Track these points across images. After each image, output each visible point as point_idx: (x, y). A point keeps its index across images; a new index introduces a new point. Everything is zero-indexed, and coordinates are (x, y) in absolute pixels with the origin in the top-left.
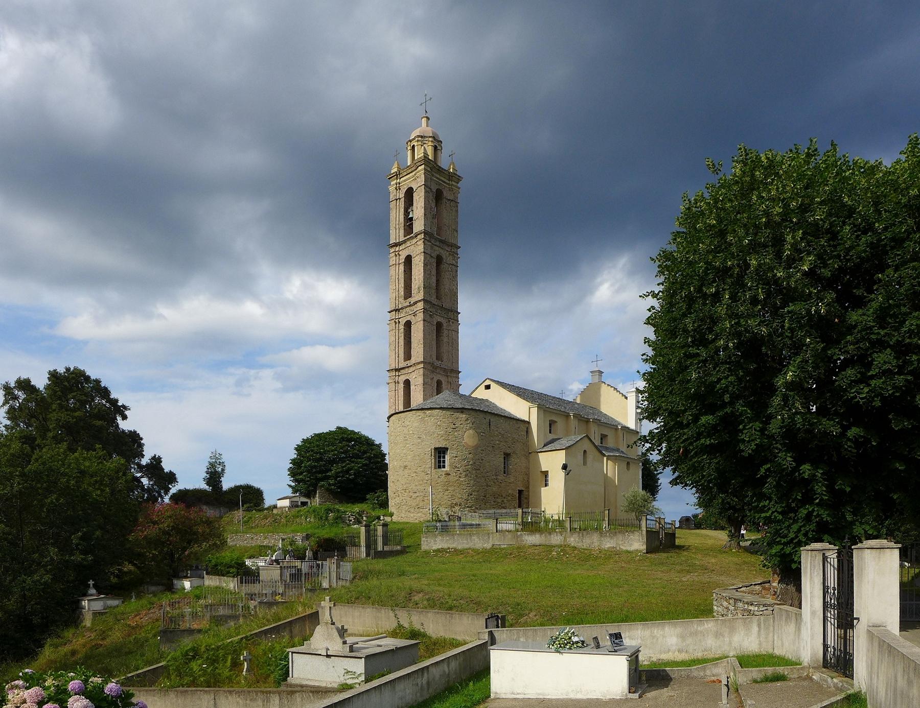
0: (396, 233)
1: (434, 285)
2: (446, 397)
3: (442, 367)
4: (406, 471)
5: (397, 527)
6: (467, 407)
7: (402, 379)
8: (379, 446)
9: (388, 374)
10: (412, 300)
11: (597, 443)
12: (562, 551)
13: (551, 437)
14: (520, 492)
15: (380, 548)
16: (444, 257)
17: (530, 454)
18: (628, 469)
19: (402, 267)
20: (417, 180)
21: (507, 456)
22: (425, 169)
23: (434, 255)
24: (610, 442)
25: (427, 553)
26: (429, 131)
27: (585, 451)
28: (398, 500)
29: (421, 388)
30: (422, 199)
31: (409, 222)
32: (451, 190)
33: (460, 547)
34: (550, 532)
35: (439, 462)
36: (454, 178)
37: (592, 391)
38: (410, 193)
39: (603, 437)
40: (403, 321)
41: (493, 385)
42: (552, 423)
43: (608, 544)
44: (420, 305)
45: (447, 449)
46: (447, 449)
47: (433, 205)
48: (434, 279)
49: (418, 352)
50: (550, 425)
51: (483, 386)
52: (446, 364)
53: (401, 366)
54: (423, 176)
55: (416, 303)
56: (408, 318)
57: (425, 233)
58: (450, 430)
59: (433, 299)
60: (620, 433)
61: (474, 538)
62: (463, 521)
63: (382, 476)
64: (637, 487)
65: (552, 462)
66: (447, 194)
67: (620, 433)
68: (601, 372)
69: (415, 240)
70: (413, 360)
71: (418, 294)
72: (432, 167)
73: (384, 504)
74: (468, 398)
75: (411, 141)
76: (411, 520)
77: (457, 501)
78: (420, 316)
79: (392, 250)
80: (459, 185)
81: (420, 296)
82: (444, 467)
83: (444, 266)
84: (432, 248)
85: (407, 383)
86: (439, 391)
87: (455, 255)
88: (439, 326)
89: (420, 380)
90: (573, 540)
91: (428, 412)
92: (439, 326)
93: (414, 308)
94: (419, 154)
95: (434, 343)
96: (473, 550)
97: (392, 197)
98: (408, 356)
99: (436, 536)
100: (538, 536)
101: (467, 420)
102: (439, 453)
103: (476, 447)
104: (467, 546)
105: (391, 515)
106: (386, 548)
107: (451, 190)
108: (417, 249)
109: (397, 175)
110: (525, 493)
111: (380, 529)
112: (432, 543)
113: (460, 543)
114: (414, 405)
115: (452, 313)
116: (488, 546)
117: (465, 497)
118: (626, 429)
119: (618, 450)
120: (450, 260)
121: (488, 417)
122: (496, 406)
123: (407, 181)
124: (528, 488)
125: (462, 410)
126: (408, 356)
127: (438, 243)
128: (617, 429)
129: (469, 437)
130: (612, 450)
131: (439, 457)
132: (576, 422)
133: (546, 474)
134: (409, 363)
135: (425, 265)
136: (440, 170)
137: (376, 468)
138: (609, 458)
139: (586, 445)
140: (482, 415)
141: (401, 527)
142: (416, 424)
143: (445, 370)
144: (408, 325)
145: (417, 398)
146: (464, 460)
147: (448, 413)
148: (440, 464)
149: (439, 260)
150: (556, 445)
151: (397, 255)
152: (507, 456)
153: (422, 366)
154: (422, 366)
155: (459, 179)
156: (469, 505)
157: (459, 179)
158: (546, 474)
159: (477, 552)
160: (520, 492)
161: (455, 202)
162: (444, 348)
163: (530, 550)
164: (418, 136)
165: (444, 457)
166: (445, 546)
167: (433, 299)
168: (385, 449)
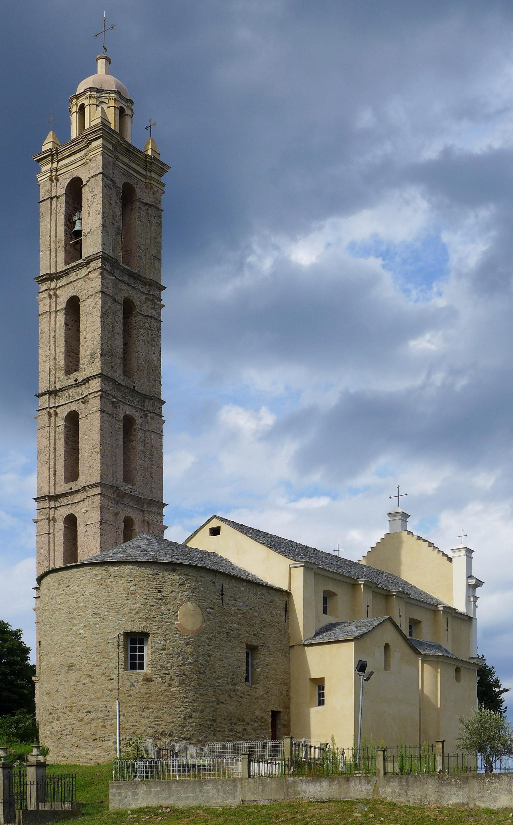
0: (50, 256)
1: (120, 350)
2: (140, 545)
3: (133, 496)
4: (73, 674)
5: (58, 772)
6: (182, 561)
7: (62, 513)
8: (17, 634)
9: (35, 505)
10: (80, 376)
11: (406, 631)
12: (371, 810)
13: (328, 619)
14: (275, 714)
15: (31, 806)
16: (137, 303)
17: (291, 649)
18: (458, 678)
19: (61, 318)
20: (89, 166)
21: (252, 650)
22: (103, 146)
23: (120, 298)
24: (425, 634)
25: (120, 815)
26: (110, 82)
27: (387, 646)
28: (56, 726)
29: (96, 530)
30: (99, 199)
31: (74, 238)
32: (148, 187)
33: (181, 805)
34: (347, 777)
35: (133, 658)
36: (154, 166)
37: (389, 545)
38: (75, 188)
39: (414, 624)
40: (63, 412)
41: (225, 528)
42: (328, 597)
43: (454, 797)
44: (96, 385)
45: (147, 635)
46: (147, 635)
47: (118, 211)
48: (119, 341)
49: (91, 466)
50: (325, 599)
51: (206, 530)
52: (140, 490)
53: (60, 490)
54: (100, 158)
55: (86, 381)
56: (73, 407)
57: (104, 257)
58: (151, 601)
59: (118, 375)
60: (442, 619)
61: (209, 787)
62: (182, 760)
63: (22, 687)
64: (474, 709)
65: (333, 664)
66: (141, 194)
67: (442, 619)
68: (405, 516)
69: (84, 271)
70: (82, 481)
71: (90, 365)
72: (116, 145)
73: (31, 735)
74: (182, 549)
75: (77, 97)
76: (81, 762)
77: (164, 727)
78: (95, 404)
79: (43, 287)
80: (163, 179)
81: (96, 368)
82: (141, 667)
83: (136, 319)
84: (116, 285)
85: (71, 522)
86: (127, 537)
87: (156, 303)
88: (128, 423)
89: (95, 516)
90: (390, 792)
91: (113, 569)
92: (128, 423)
93: (84, 390)
94: (93, 119)
95: (120, 452)
96: (206, 809)
97: (43, 193)
98: (72, 473)
99: (136, 785)
100: (325, 784)
101: (183, 584)
102: (133, 642)
103: (199, 633)
104: (195, 803)
105: (44, 752)
106: (44, 807)
107: (148, 187)
108: (89, 286)
109: (53, 155)
110: (283, 717)
111: (31, 773)
112: (130, 798)
113: (181, 797)
114: (82, 558)
115: (151, 402)
116: (234, 802)
117: (179, 721)
118: (450, 611)
119: (439, 647)
120: (147, 309)
121: (220, 581)
122: (231, 565)
123: (71, 167)
124: (288, 707)
125: (174, 567)
126: (72, 473)
127: (126, 279)
128: (436, 611)
129: (187, 616)
130: (431, 646)
131: (133, 650)
132: (369, 595)
133: (319, 684)
134: (74, 486)
135: (104, 315)
136: (130, 151)
137: (13, 673)
138: (426, 659)
139: (389, 634)
140: (208, 578)
141: (66, 772)
142: (90, 590)
143: (139, 500)
144: (73, 418)
145: (89, 546)
146: (178, 654)
147: (150, 571)
148: (135, 662)
149: (128, 307)
150: (337, 633)
151: (53, 295)
152: (252, 650)
153: (98, 490)
154: (98, 490)
155: (163, 169)
156: (186, 735)
157: (163, 169)
158: (319, 684)
159: (213, 813)
160: (275, 714)
161: (155, 208)
162: (138, 462)
163: (313, 810)
164: (91, 89)
165: (142, 650)
166: (152, 802)
167: (118, 375)
168: (28, 639)
